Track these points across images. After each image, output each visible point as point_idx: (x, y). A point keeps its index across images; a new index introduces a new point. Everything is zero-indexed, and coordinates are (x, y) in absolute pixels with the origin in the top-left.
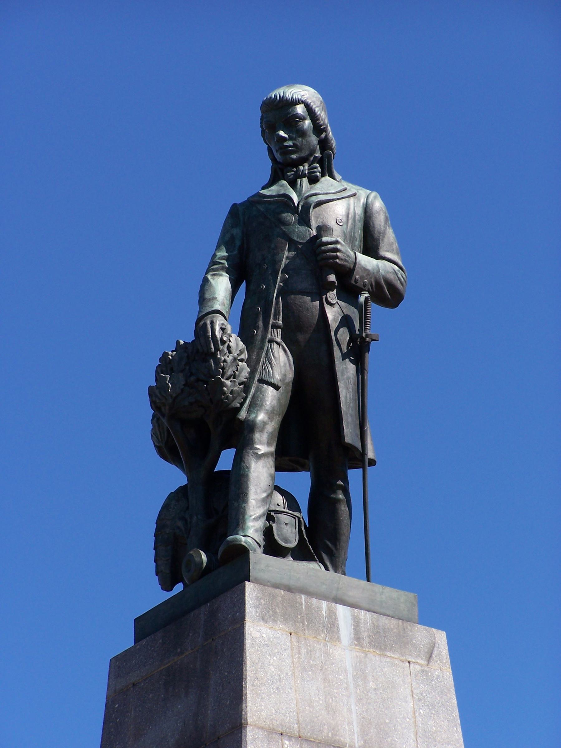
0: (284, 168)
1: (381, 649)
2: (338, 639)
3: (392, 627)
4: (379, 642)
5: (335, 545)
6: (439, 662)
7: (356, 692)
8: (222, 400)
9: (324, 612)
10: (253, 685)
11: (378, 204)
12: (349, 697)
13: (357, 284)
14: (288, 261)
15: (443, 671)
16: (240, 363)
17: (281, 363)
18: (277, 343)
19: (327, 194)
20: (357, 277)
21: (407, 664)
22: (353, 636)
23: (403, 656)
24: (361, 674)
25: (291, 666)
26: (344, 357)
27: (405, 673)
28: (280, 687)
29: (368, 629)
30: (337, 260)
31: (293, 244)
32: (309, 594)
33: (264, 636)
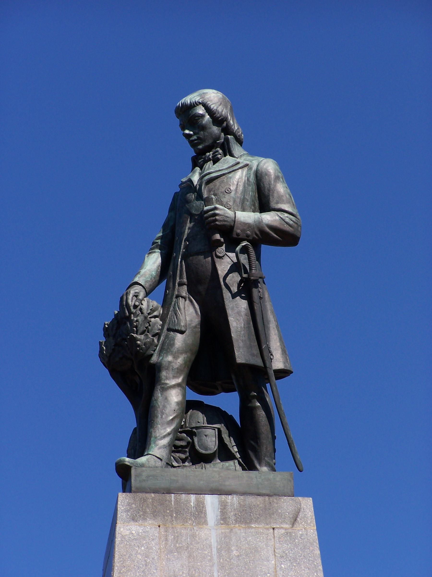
0: (198, 161)
1: (246, 523)
2: (206, 522)
3: (258, 503)
4: (245, 517)
5: (257, 443)
6: (303, 523)
7: (220, 562)
8: (138, 351)
9: (192, 504)
10: (120, 573)
11: (270, 166)
12: (213, 566)
13: (240, 237)
14: (190, 230)
15: (308, 529)
16: (153, 320)
17: (189, 313)
18: (184, 298)
19: (219, 171)
20: (239, 231)
21: (272, 530)
22: (219, 517)
23: (267, 524)
24: (225, 546)
25: (157, 552)
26: (234, 296)
27: (269, 538)
28: (146, 570)
29: (235, 509)
30: (217, 223)
31: (192, 215)
32: (188, 492)
33: (134, 532)
